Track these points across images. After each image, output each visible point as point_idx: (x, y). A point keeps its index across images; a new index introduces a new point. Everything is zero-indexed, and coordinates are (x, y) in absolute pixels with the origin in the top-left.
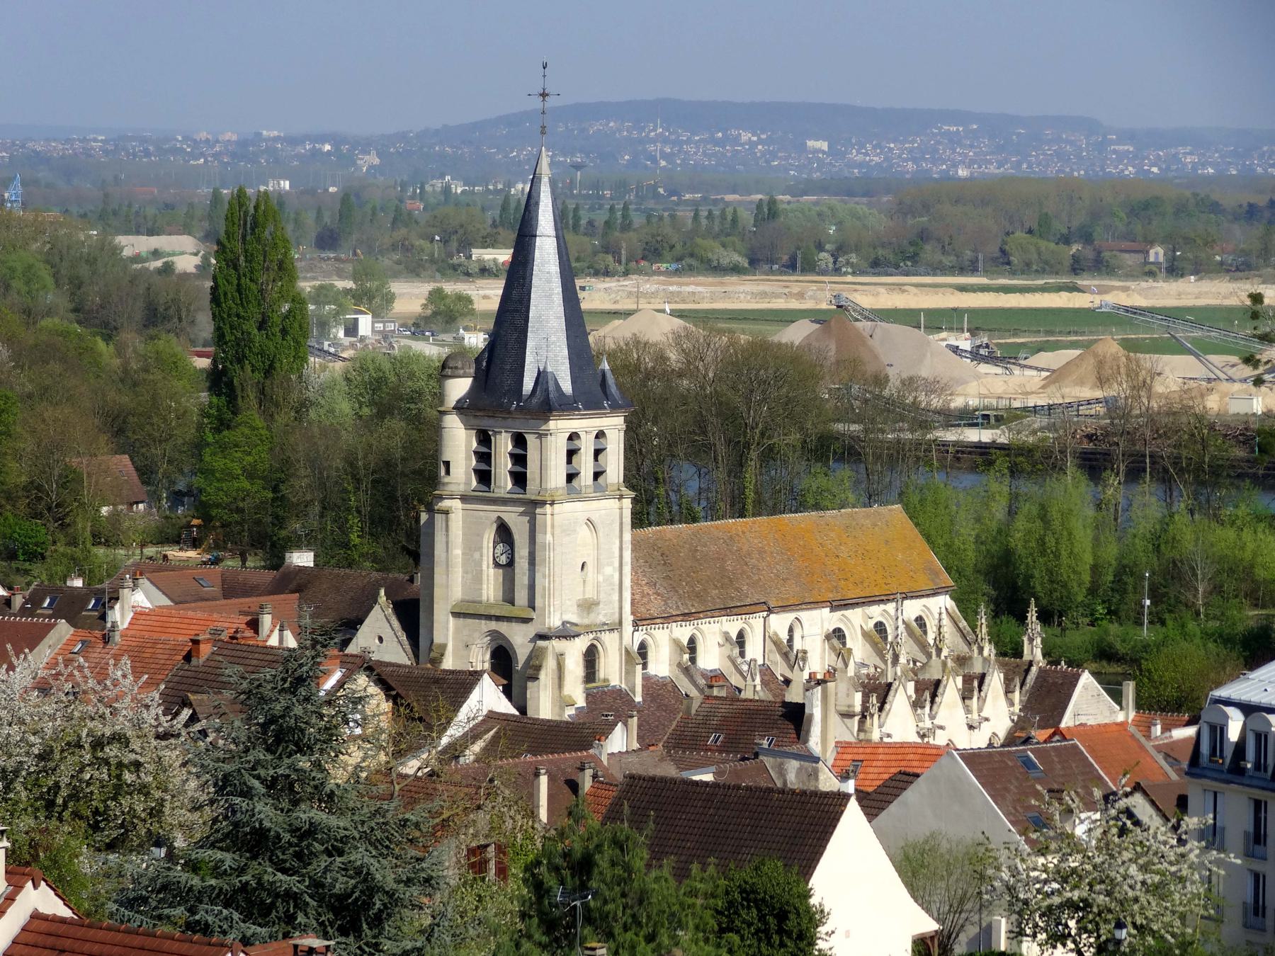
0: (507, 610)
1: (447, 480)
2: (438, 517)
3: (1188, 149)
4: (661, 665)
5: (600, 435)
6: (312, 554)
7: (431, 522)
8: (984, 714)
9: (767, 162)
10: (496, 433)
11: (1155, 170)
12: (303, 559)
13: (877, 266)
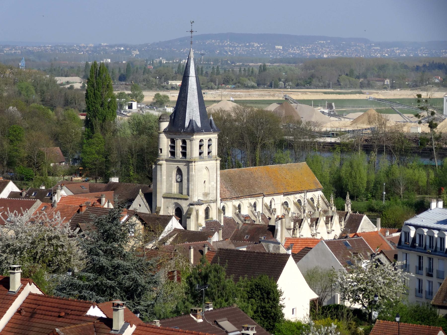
0: (180, 196)
1: (161, 154)
3: (397, 48)
4: (229, 213)
5: (210, 140)
7: (156, 168)
8: (332, 229)
11: (387, 55)
12: (115, 180)
13: (298, 86)
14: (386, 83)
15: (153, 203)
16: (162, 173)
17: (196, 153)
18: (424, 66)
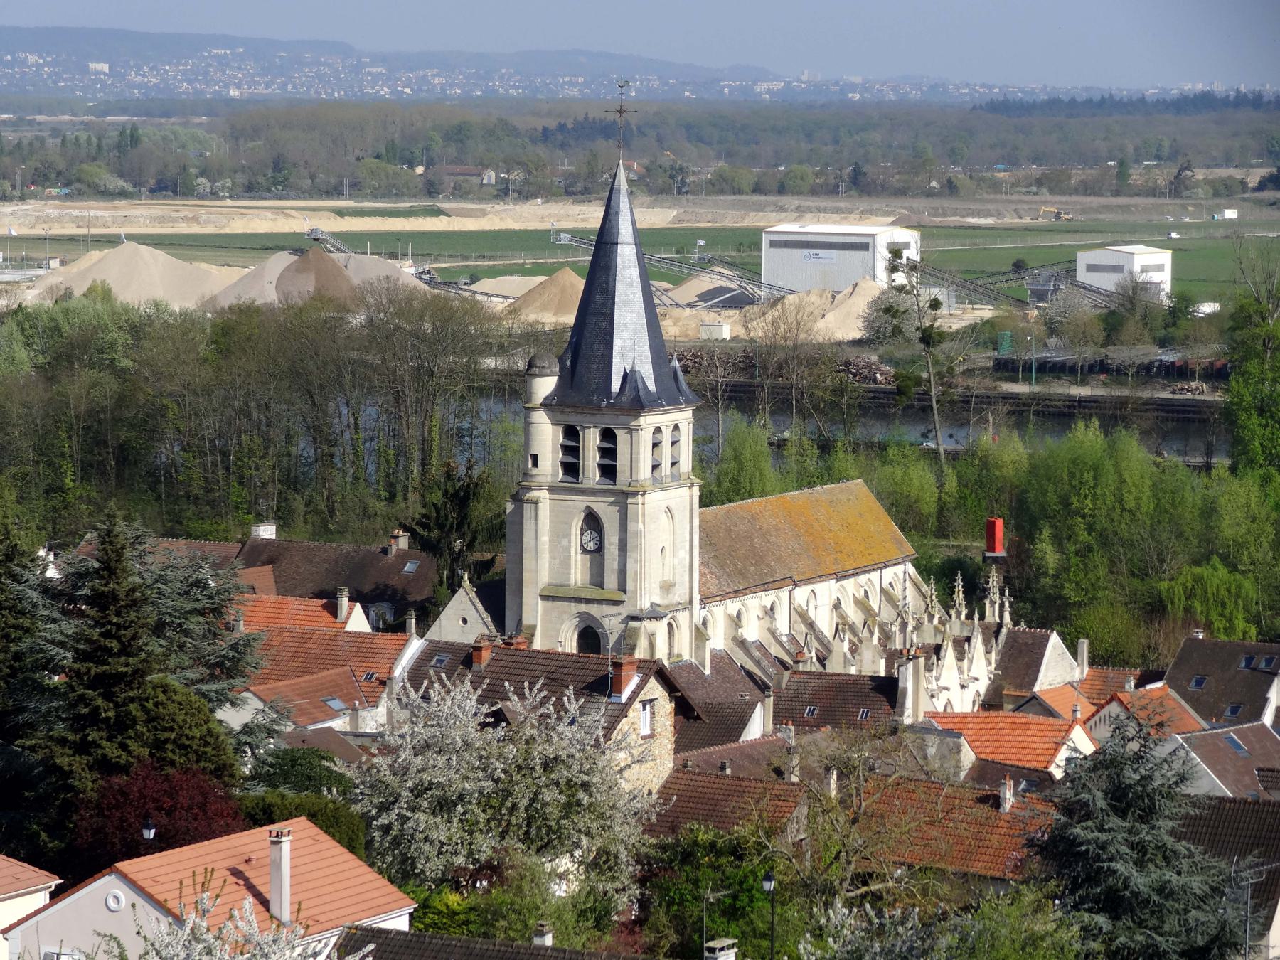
0: (596, 593)
1: (535, 471)
2: (528, 509)
3: (435, 71)
4: (718, 640)
5: (676, 427)
6: (274, 527)
7: (519, 513)
8: (972, 674)
9: (55, 82)
10: (584, 428)
11: (408, 90)
12: (267, 532)
13: (251, 190)
14: (485, 182)
15: (508, 613)
16: (540, 523)
17: (644, 471)
18: (562, 127)
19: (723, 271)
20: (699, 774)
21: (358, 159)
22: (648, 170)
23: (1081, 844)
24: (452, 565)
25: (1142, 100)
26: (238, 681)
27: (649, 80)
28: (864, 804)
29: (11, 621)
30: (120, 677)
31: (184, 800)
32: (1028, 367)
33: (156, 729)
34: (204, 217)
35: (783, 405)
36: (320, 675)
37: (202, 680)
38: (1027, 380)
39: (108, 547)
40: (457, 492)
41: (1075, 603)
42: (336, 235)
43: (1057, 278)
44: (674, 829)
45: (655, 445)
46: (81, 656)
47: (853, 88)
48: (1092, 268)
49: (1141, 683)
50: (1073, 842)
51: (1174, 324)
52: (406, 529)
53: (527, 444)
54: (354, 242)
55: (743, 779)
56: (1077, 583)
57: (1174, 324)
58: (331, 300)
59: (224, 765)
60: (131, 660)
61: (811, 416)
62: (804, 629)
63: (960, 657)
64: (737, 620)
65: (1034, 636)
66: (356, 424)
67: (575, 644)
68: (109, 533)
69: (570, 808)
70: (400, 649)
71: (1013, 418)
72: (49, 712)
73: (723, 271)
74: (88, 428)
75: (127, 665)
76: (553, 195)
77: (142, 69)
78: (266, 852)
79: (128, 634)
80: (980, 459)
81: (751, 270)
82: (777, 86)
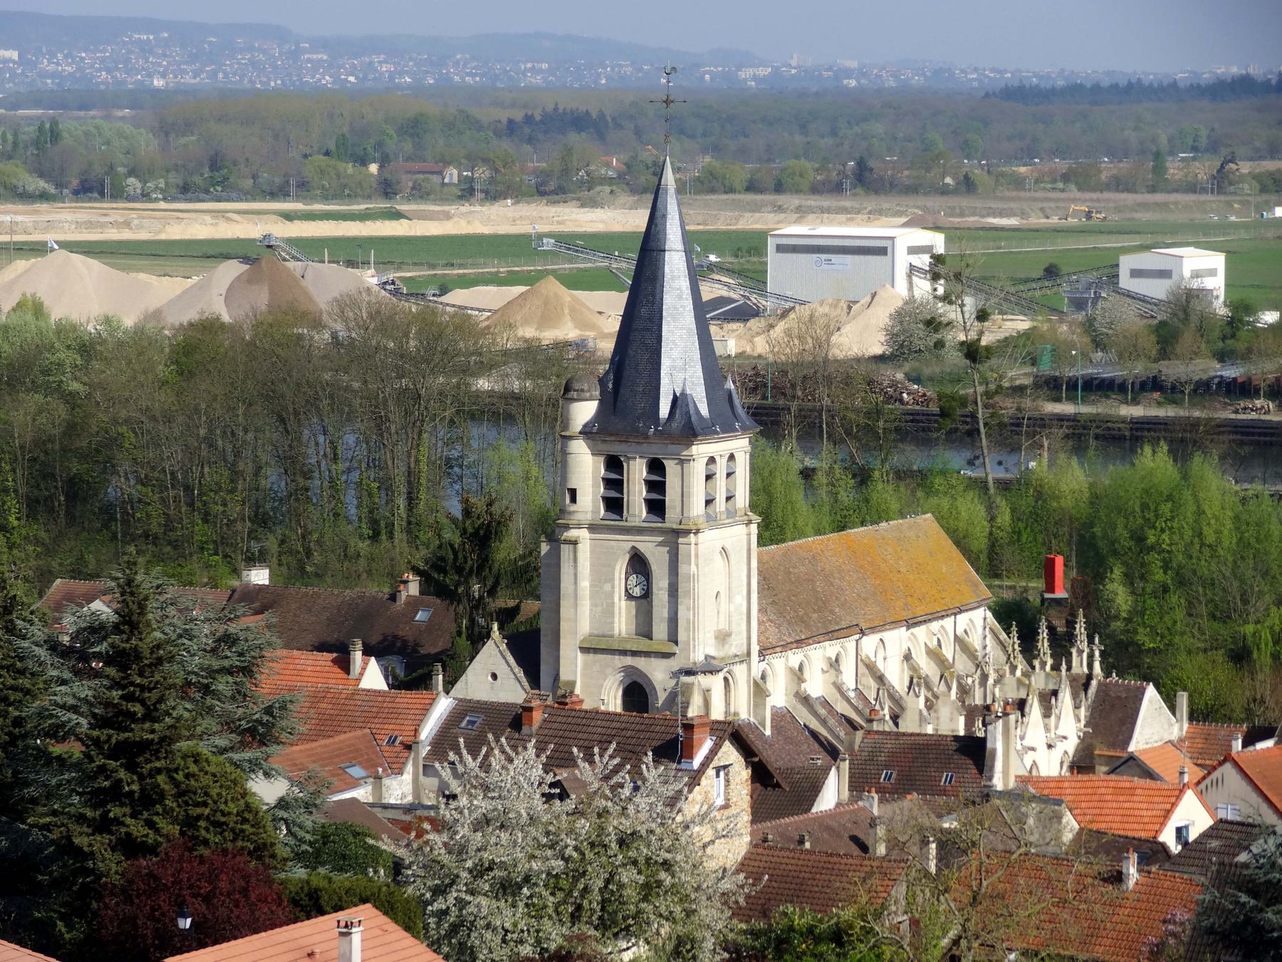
0: (643, 645)
1: (573, 508)
2: (566, 550)
3: (382, 57)
4: (779, 697)
8: (1061, 732)
10: (629, 459)
11: (352, 79)
12: (259, 576)
13: (186, 191)
15: (542, 667)
16: (580, 569)
18: (529, 119)
19: (724, 279)
20: (782, 849)
21: (305, 156)
22: (628, 166)
23: (1273, 930)
24: (471, 614)
25: (1174, 85)
26: (273, 749)
27: (620, 65)
28: (985, 883)
29: (10, 682)
30: (144, 746)
31: (223, 885)
32: (1072, 385)
33: (187, 803)
34: (136, 222)
35: (810, 431)
36: (337, 739)
37: (232, 748)
38: (1072, 399)
39: (129, 599)
40: (477, 530)
41: (1149, 650)
42: (291, 241)
43: (1099, 284)
44: (765, 914)
45: (708, 477)
46: (99, 722)
47: (848, 73)
48: (1136, 273)
49: (1249, 741)
50: (1260, 929)
51: (1233, 336)
52: (417, 571)
53: (564, 478)
54: (310, 248)
55: (831, 855)
56: (1151, 627)
57: (1233, 336)
58: (304, 314)
59: (264, 844)
60: (156, 726)
61: (842, 441)
62: (873, 684)
63: (1047, 713)
64: (798, 674)
65: (1128, 689)
66: (335, 455)
67: (619, 701)
68: (129, 582)
69: (649, 890)
70: (426, 710)
71: (1070, 443)
72: (59, 785)
73: (724, 279)
74: (34, 460)
75: (153, 732)
76: (524, 195)
77: (56, 57)
78: (335, 943)
79: (154, 695)
80: (1035, 490)
81: (755, 278)
82: (764, 72)
